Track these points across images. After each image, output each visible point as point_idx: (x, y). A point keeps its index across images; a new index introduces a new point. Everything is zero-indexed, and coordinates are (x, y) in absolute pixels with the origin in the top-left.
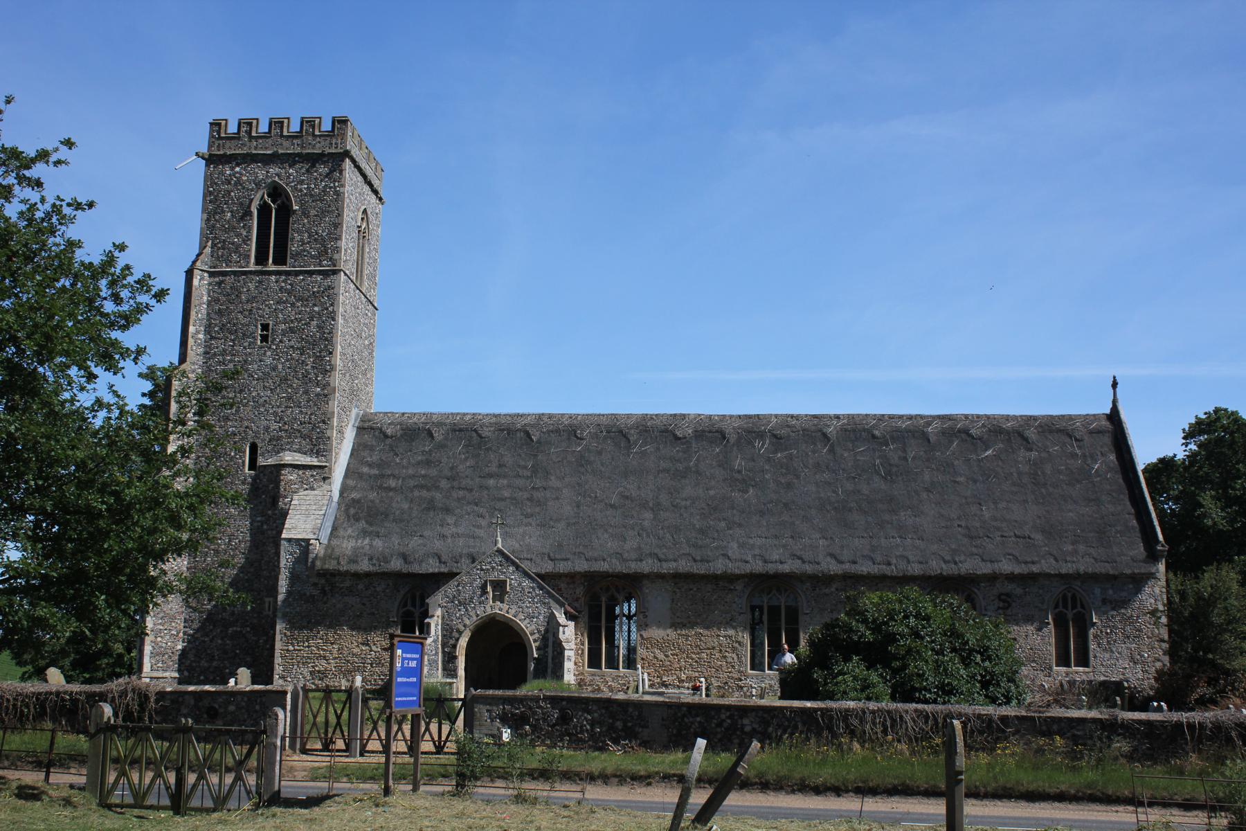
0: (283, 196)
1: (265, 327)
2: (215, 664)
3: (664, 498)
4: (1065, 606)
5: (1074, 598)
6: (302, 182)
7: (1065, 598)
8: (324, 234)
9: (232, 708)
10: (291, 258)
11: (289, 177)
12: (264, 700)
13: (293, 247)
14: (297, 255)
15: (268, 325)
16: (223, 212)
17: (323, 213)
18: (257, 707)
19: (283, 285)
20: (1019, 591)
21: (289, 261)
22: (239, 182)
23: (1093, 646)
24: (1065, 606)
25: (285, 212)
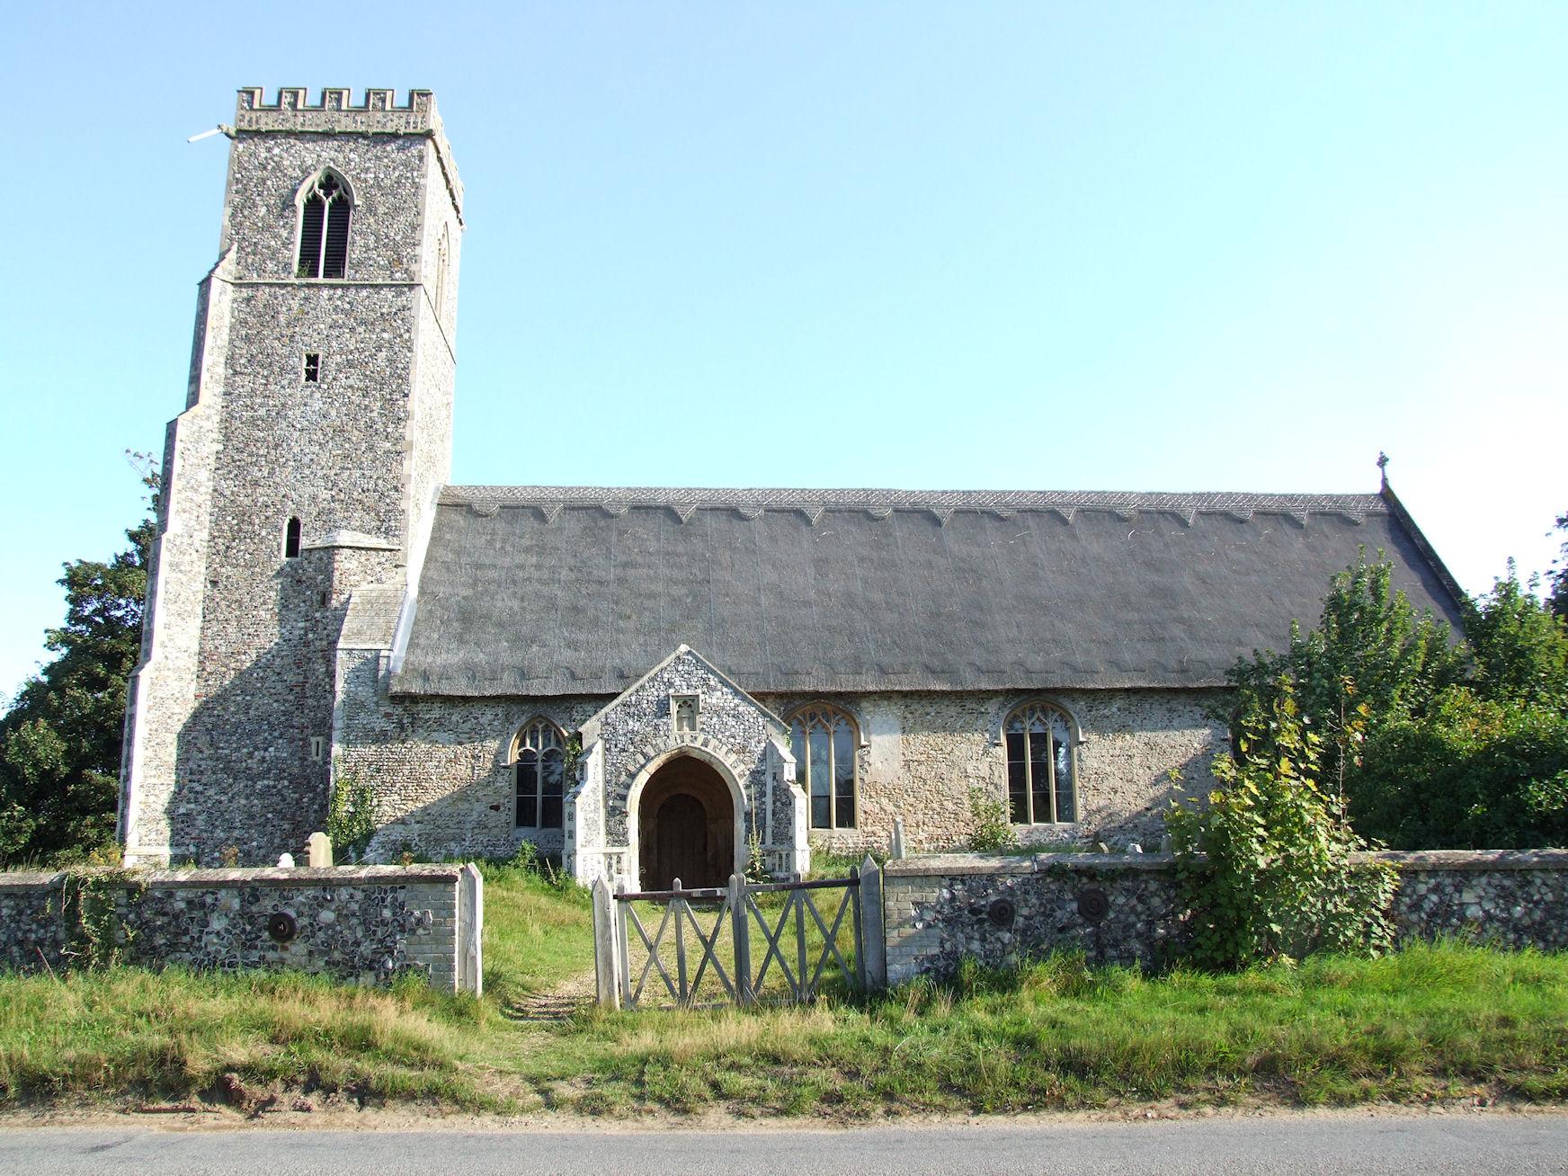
0: (341, 187)
1: (313, 360)
2: (236, 833)
6: (367, 170)
8: (398, 238)
9: (327, 916)
10: (350, 268)
11: (352, 162)
12: (401, 895)
15: (316, 357)
16: (255, 205)
17: (397, 210)
18: (387, 913)
19: (339, 303)
22: (278, 166)
25: (342, 208)
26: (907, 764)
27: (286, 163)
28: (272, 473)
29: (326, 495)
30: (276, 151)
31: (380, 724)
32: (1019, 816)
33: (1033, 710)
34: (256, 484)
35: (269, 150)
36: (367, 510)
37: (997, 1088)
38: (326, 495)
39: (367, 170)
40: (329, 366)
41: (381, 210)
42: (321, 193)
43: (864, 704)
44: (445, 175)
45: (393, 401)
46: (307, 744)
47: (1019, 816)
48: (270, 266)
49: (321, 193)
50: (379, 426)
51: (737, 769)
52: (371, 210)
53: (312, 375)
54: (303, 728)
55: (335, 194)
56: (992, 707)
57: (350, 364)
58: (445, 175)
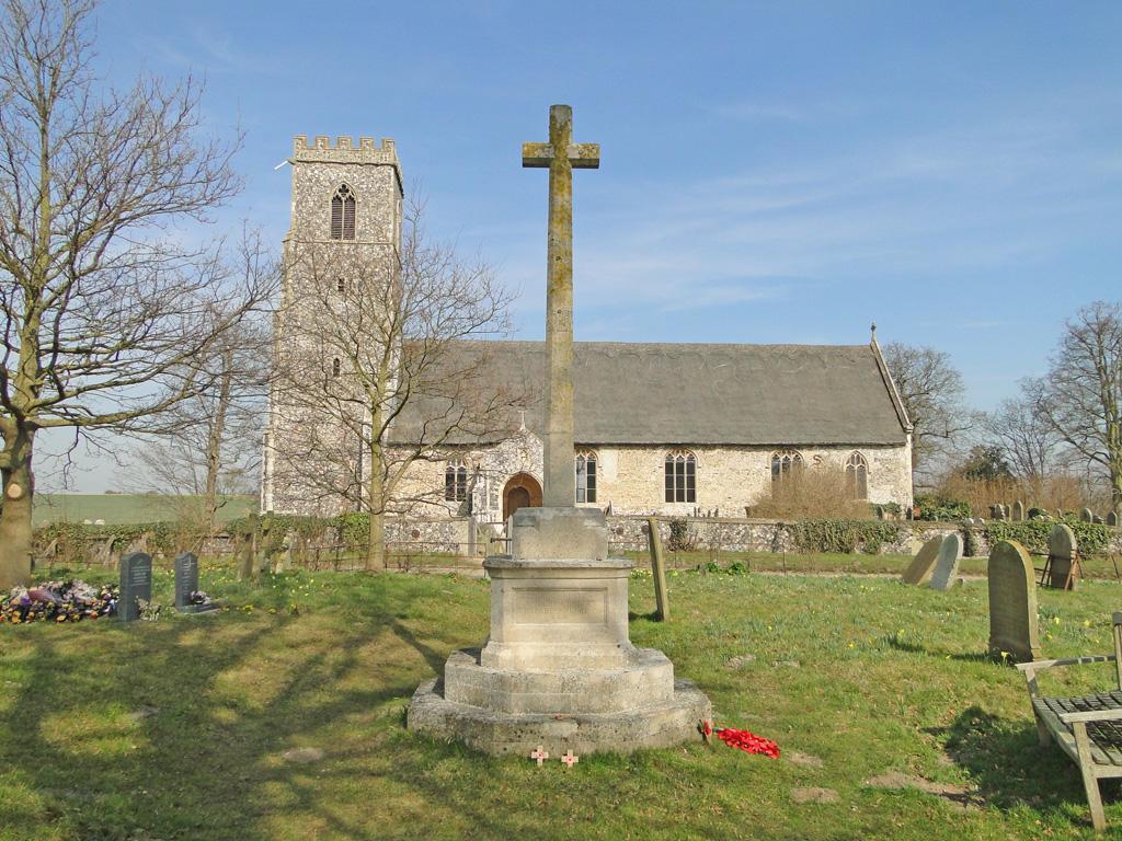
4: (853, 463)
5: (858, 457)
7: (853, 457)
13: (358, 227)
14: (361, 233)
22: (318, 180)
23: (869, 485)
26: (619, 476)
27: (322, 179)
30: (316, 172)
32: (669, 498)
35: (313, 171)
41: (371, 204)
42: (340, 195)
47: (669, 498)
52: (366, 205)
55: (347, 195)
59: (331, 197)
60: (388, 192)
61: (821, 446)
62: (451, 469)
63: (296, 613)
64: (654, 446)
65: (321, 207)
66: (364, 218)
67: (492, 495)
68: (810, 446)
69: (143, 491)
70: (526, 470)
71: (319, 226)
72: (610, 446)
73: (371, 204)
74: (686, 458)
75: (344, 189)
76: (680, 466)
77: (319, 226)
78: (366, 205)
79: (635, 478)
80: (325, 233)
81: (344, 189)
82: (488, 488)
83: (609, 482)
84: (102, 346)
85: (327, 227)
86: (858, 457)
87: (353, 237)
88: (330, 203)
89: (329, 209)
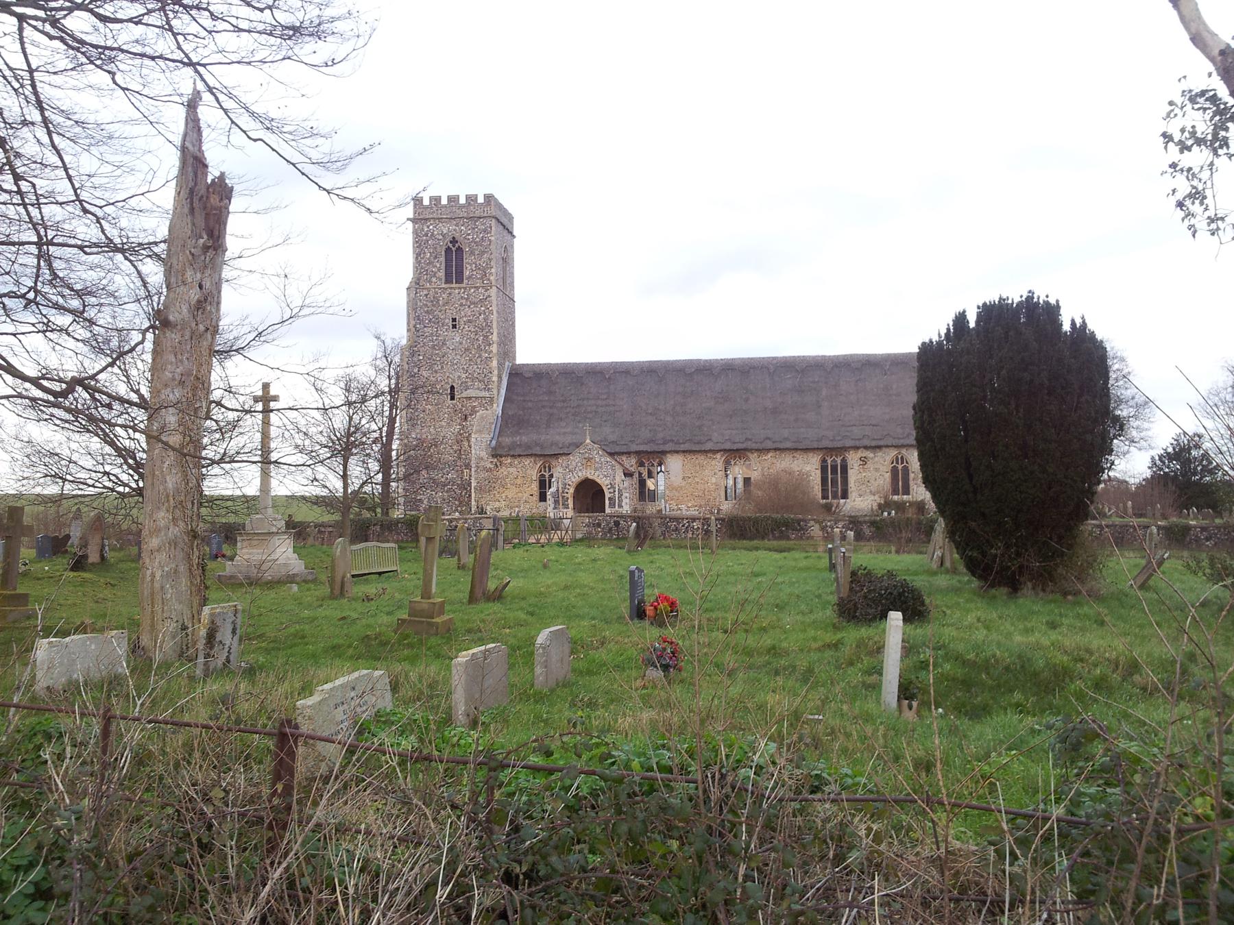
1: (454, 320)
3: (678, 408)
4: (897, 463)
5: (902, 458)
6: (469, 235)
7: (897, 458)
13: (467, 273)
14: (469, 278)
17: (483, 253)
20: (872, 455)
21: (465, 281)
22: (433, 233)
23: (911, 483)
24: (897, 463)
25: (460, 250)
26: (684, 478)
28: (442, 367)
29: (464, 376)
31: (489, 465)
33: (735, 457)
34: (436, 372)
36: (480, 381)
37: (1167, 752)
38: (464, 376)
39: (469, 235)
40: (461, 322)
41: (477, 252)
42: (451, 245)
43: (668, 455)
44: (273, 150)
45: (487, 337)
46: (463, 472)
48: (434, 280)
49: (451, 245)
50: (483, 347)
51: (603, 482)
52: (472, 253)
53: (454, 326)
54: (461, 466)
56: (718, 456)
57: (470, 321)
58: (273, 150)
59: (444, 248)
60: (490, 241)
61: (866, 448)
62: (543, 476)
63: (682, 681)
64: (715, 452)
65: (436, 257)
66: (471, 265)
67: (563, 497)
68: (857, 448)
69: (289, 494)
70: (590, 477)
71: (435, 273)
72: (677, 452)
73: (477, 252)
74: (839, 461)
75: (454, 241)
76: (834, 469)
77: (435, 273)
78: (472, 253)
79: (697, 479)
80: (441, 280)
81: (454, 241)
82: (560, 491)
83: (675, 484)
84: (110, 480)
85: (442, 274)
86: (902, 458)
87: (462, 282)
88: (443, 253)
89: (443, 259)
